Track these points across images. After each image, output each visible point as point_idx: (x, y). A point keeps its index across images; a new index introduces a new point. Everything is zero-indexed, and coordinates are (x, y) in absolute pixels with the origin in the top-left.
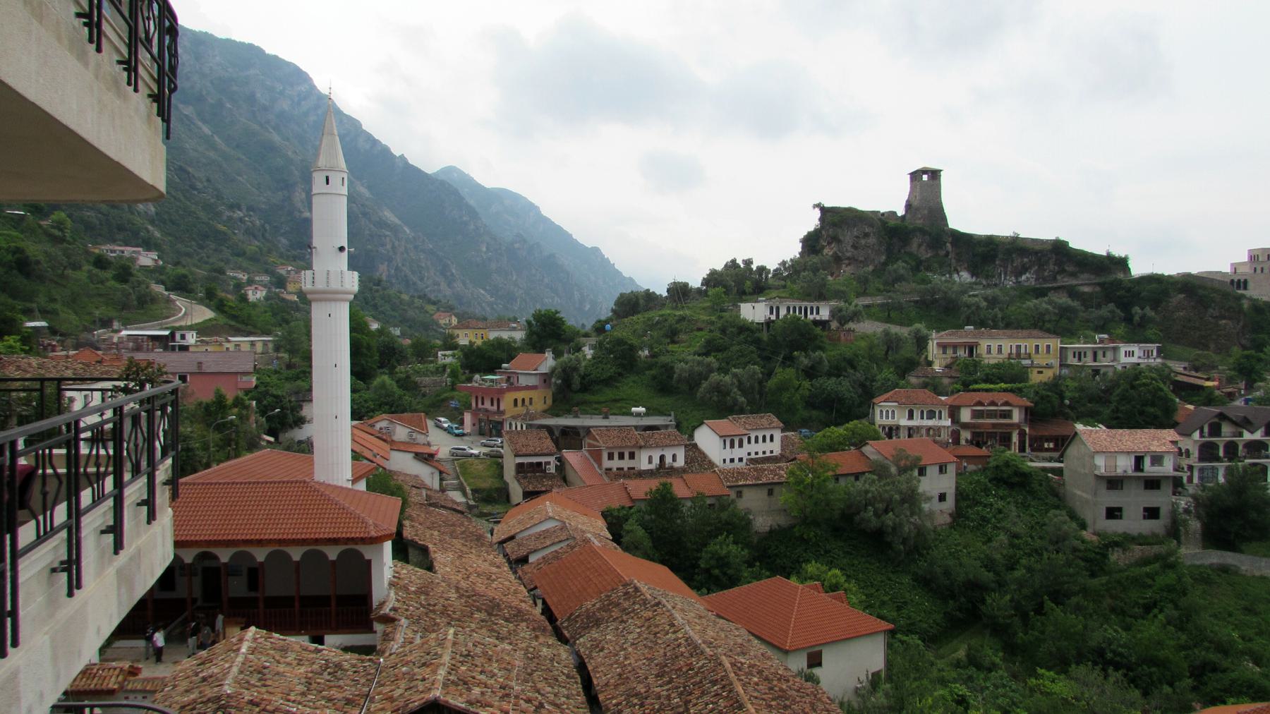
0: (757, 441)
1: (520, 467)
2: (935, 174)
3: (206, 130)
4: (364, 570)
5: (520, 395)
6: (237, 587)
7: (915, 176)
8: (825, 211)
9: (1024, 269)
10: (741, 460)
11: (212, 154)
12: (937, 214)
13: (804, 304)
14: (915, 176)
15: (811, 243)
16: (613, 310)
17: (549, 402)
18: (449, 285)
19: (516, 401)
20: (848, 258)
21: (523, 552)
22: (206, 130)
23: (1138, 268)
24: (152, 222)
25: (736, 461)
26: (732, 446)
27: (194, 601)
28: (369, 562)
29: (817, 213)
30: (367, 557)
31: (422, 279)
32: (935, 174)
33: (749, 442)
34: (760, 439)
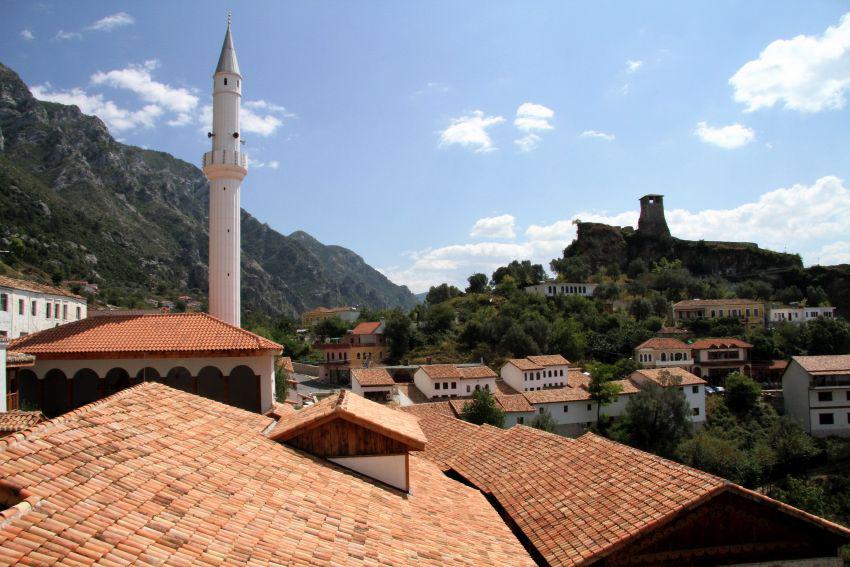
2: (658, 199)
3: (133, 209)
5: (361, 350)
7: (644, 201)
9: (729, 265)
11: (136, 225)
12: (662, 226)
13: (573, 285)
14: (644, 201)
16: (477, 282)
19: (359, 355)
20: (600, 260)
23: (808, 263)
24: (95, 268)
29: (575, 228)
32: (658, 199)
33: (545, 376)
34: (559, 373)
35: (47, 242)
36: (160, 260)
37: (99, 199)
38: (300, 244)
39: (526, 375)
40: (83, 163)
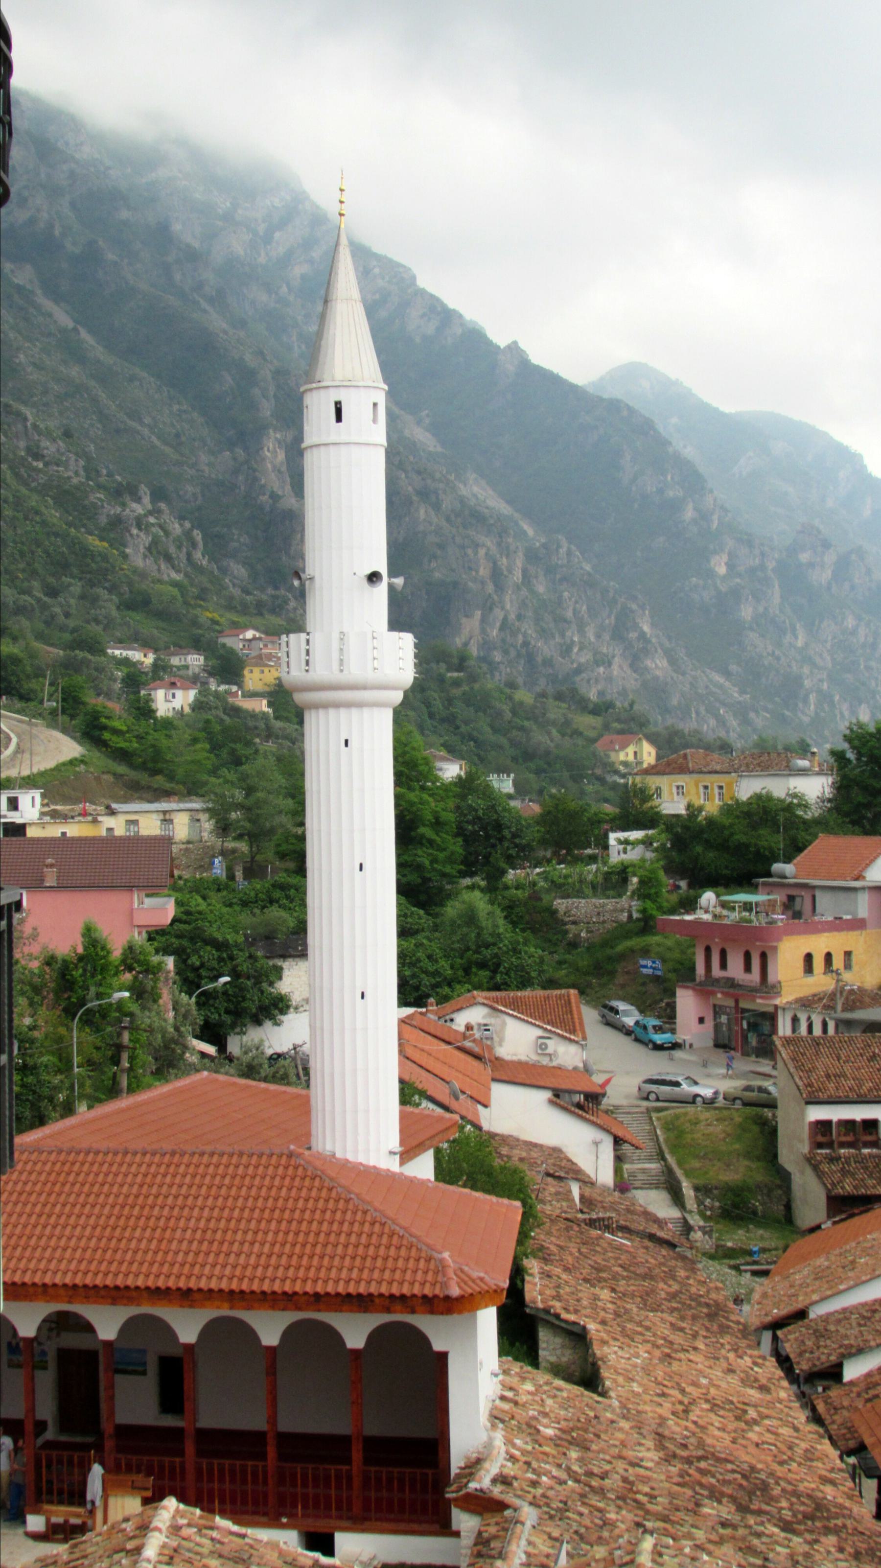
3: (63, 318)
18: (635, 662)
19: (809, 958)
21: (826, 1357)
28: (443, 1357)
36: (158, 495)
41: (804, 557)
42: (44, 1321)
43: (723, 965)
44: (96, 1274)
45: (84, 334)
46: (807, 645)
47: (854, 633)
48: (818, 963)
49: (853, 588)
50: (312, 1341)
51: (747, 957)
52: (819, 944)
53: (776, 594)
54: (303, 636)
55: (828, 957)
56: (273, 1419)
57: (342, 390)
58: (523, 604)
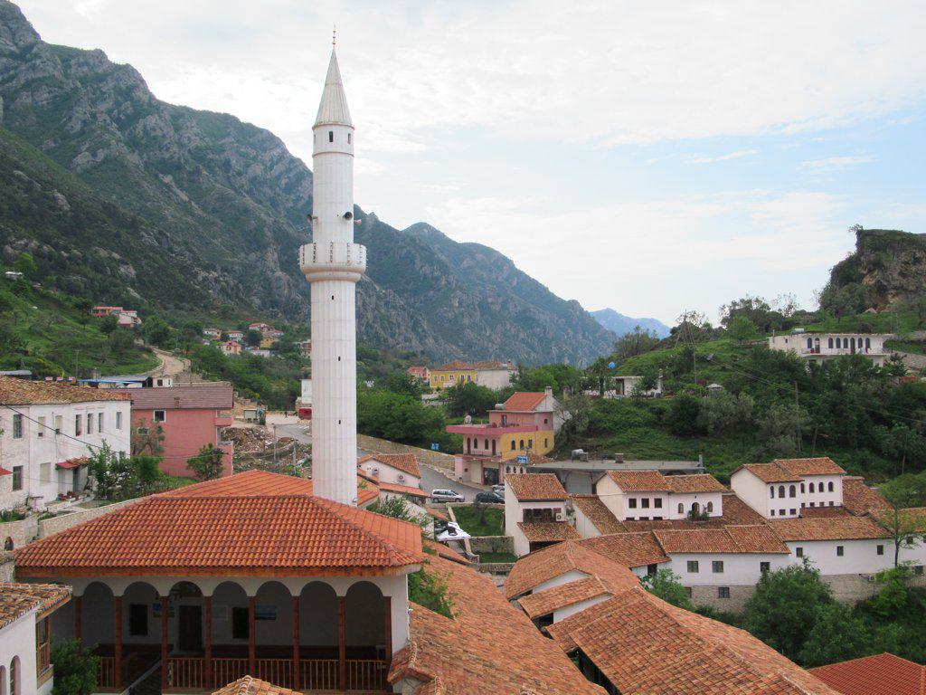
0: (812, 490)
1: (527, 513)
3: (184, 196)
4: (380, 609)
6: (219, 630)
8: (862, 235)
10: (793, 511)
15: (844, 274)
17: (551, 445)
18: (421, 340)
19: (513, 443)
20: (895, 288)
21: (546, 609)
22: (184, 196)
25: (777, 513)
26: (782, 495)
27: (170, 648)
28: (388, 600)
29: (854, 239)
30: (385, 594)
31: (393, 336)
33: (803, 491)
34: (817, 488)
35: (67, 250)
36: (224, 269)
37: (137, 183)
38: (423, 242)
39: (772, 489)
40: (113, 134)
41: (490, 300)
42: (172, 590)
43: (476, 447)
44: (202, 560)
45: (193, 203)
46: (490, 335)
47: (510, 330)
48: (518, 445)
49: (509, 313)
50: (318, 591)
51: (487, 442)
52: (517, 437)
53: (478, 314)
54: (312, 245)
55: (522, 442)
56: (297, 637)
57: (333, 127)
58: (375, 317)
